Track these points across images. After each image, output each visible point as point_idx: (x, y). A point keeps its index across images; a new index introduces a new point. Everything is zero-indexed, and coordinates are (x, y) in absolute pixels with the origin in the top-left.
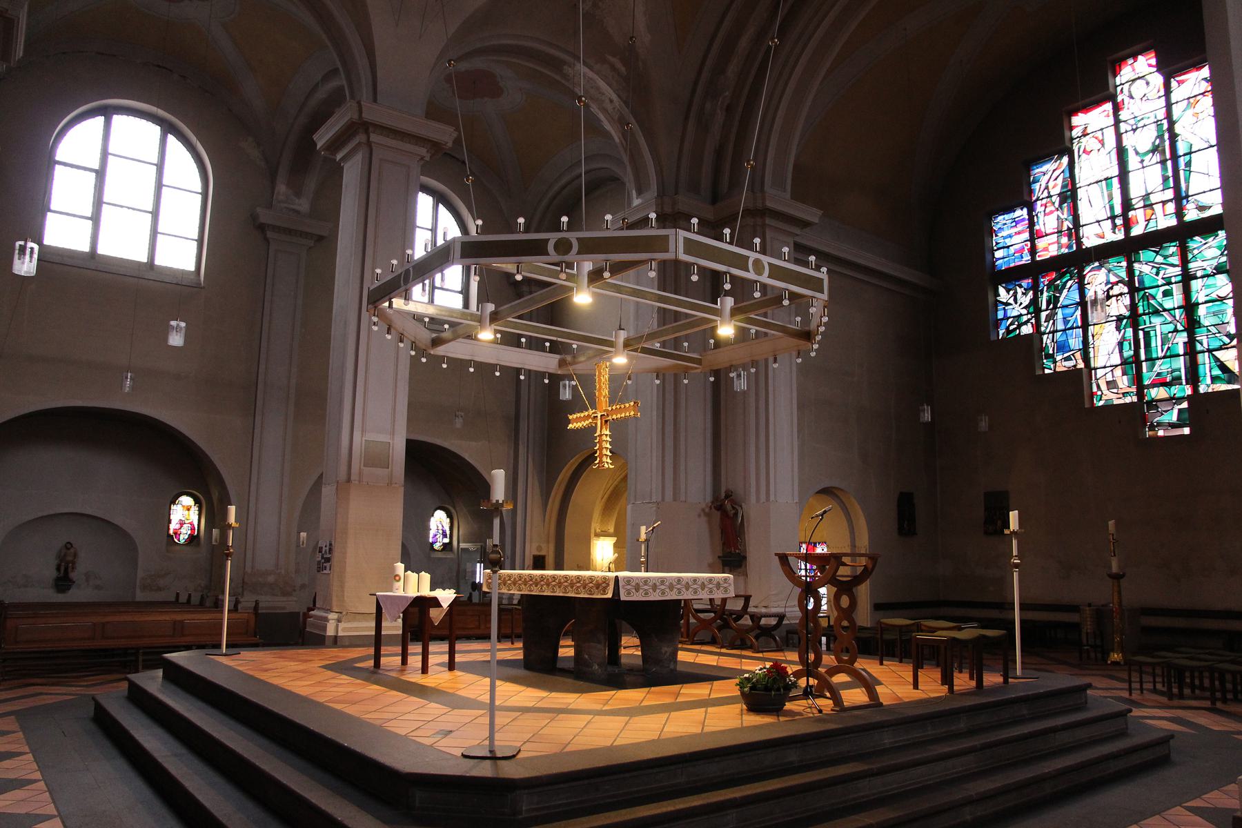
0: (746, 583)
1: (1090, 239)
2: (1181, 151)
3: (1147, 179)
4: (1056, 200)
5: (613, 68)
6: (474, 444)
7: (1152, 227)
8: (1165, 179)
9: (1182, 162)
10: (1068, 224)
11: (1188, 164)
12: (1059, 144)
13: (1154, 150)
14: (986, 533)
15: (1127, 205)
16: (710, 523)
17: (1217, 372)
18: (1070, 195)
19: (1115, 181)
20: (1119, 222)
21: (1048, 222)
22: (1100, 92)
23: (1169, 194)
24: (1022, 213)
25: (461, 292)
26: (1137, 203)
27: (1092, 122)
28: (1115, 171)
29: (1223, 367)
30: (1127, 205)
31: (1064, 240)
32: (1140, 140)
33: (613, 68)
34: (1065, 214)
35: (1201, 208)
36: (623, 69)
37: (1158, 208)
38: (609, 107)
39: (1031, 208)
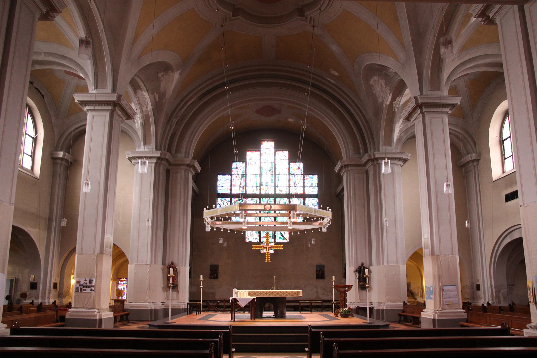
0: (177, 294)
1: (250, 191)
2: (276, 173)
3: (267, 178)
4: (240, 176)
5: (155, 97)
6: (35, 230)
7: (267, 193)
8: (272, 180)
9: (277, 176)
10: (243, 184)
11: (278, 177)
12: (242, 159)
13: (270, 171)
14: (211, 278)
15: (261, 184)
16: (163, 272)
17: (281, 236)
18: (244, 176)
19: (259, 176)
20: (258, 188)
21: (237, 181)
22: (256, 147)
23: (273, 184)
24: (228, 177)
25: (31, 156)
26: (264, 184)
27: (251, 155)
28: (259, 173)
29: (282, 236)
30: (261, 184)
31: (241, 189)
32: (267, 167)
33: (155, 97)
34: (243, 181)
35: (281, 191)
36: (157, 99)
37: (269, 187)
38: (144, 109)
39: (231, 175)
